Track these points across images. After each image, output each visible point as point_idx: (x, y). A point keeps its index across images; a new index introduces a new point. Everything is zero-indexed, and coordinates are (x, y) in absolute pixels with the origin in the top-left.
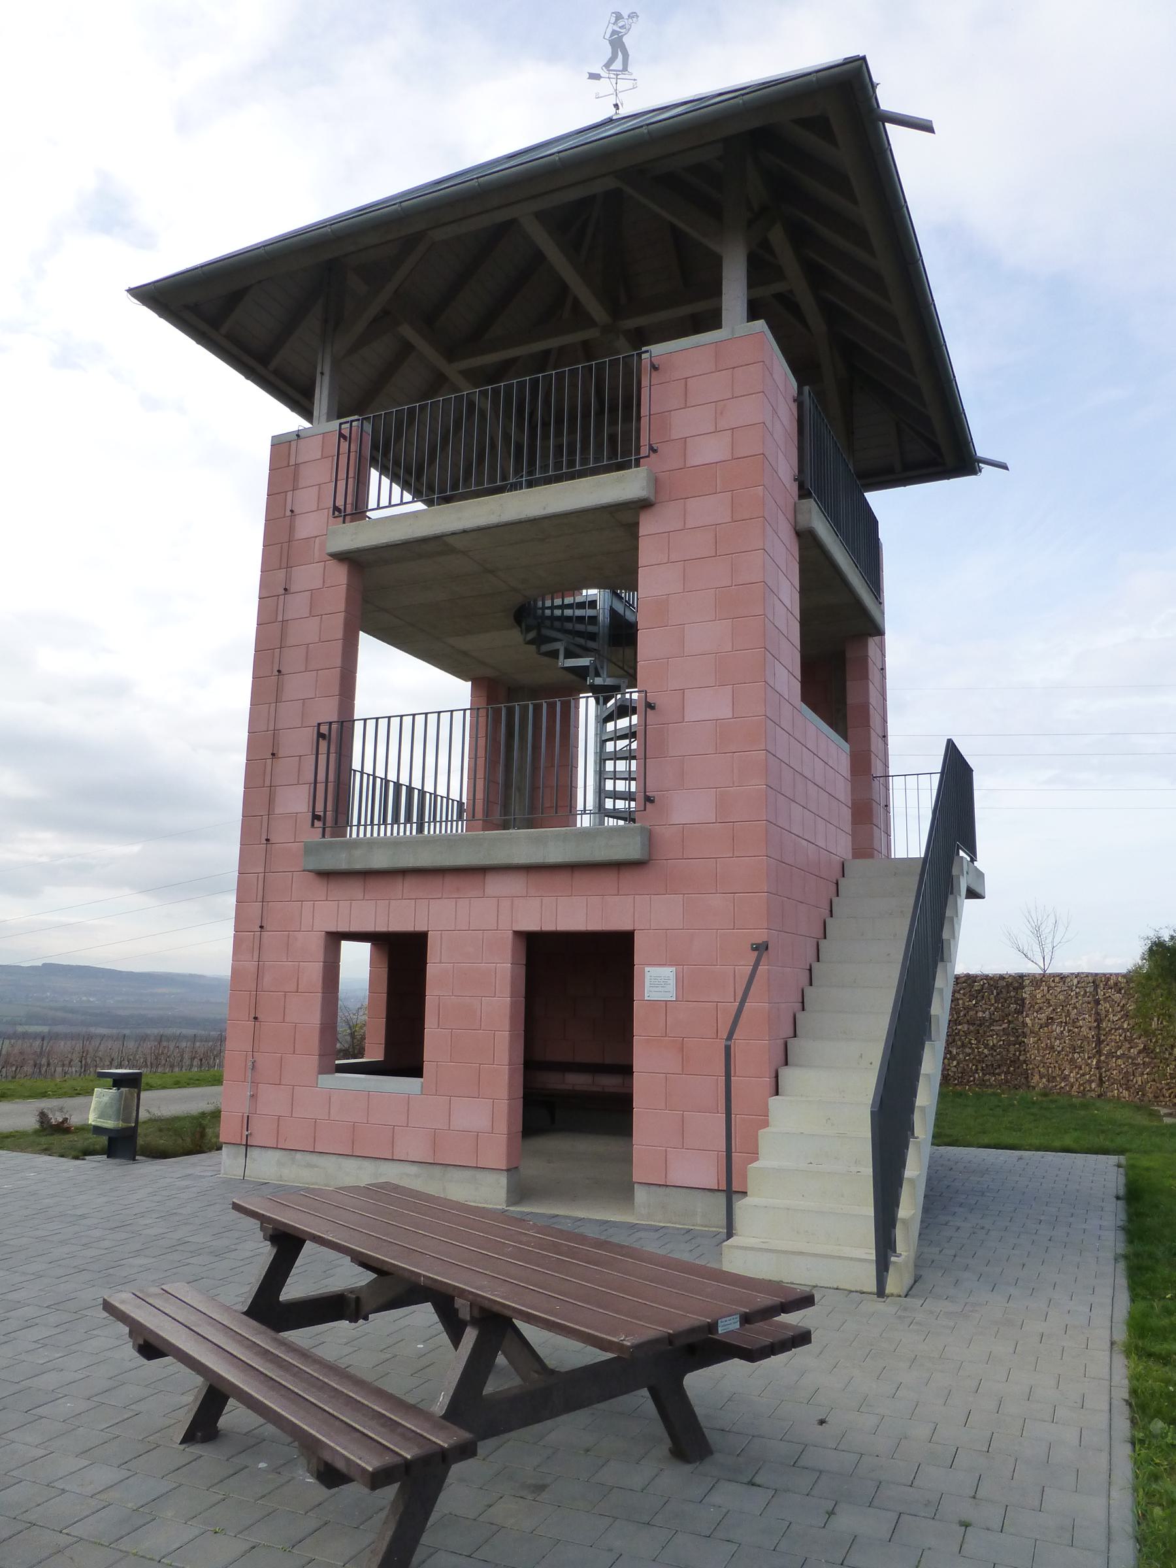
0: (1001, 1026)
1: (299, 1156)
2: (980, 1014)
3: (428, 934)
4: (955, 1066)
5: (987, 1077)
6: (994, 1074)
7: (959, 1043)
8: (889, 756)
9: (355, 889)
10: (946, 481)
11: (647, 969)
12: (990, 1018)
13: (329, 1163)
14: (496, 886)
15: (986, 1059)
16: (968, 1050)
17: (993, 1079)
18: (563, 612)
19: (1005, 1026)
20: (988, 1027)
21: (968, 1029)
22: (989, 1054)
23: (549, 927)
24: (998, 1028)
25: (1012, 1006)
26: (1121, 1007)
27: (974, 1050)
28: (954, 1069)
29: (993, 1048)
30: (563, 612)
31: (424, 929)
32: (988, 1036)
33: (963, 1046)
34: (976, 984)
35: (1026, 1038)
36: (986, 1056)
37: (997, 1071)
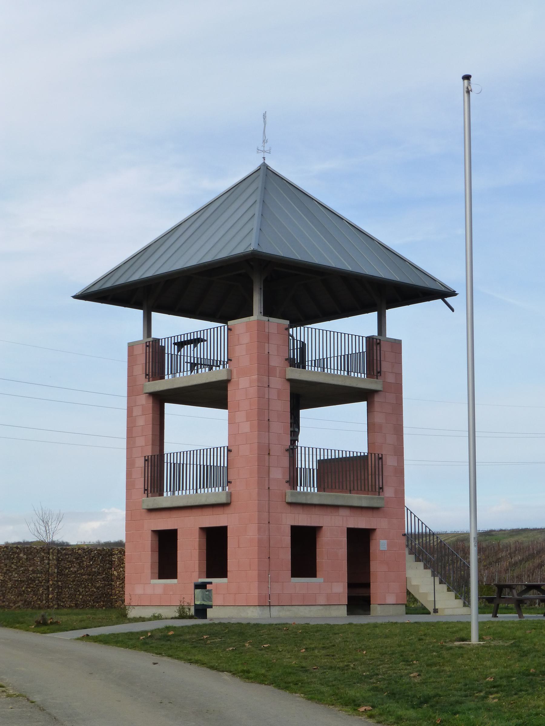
0: (101, 576)
1: (285, 607)
2: (94, 570)
3: (227, 527)
4: (81, 599)
5: (95, 604)
6: (97, 602)
7: (83, 586)
8: (165, 443)
9: (299, 510)
10: (210, 322)
11: (381, 540)
12: (98, 572)
13: (294, 609)
14: (342, 512)
15: (95, 594)
16: (87, 590)
17: (98, 604)
18: (157, 362)
19: (104, 576)
20: (97, 576)
21: (88, 578)
22: (96, 591)
23: (356, 527)
24: (101, 577)
25: (107, 565)
26: (446, 549)
27: (90, 590)
28: (80, 600)
29: (98, 588)
30: (157, 362)
31: (226, 525)
32: (96, 582)
33: (85, 587)
34: (92, 553)
35: (113, 581)
36: (95, 593)
37: (99, 600)
